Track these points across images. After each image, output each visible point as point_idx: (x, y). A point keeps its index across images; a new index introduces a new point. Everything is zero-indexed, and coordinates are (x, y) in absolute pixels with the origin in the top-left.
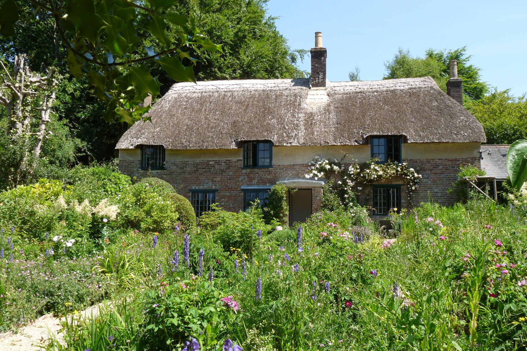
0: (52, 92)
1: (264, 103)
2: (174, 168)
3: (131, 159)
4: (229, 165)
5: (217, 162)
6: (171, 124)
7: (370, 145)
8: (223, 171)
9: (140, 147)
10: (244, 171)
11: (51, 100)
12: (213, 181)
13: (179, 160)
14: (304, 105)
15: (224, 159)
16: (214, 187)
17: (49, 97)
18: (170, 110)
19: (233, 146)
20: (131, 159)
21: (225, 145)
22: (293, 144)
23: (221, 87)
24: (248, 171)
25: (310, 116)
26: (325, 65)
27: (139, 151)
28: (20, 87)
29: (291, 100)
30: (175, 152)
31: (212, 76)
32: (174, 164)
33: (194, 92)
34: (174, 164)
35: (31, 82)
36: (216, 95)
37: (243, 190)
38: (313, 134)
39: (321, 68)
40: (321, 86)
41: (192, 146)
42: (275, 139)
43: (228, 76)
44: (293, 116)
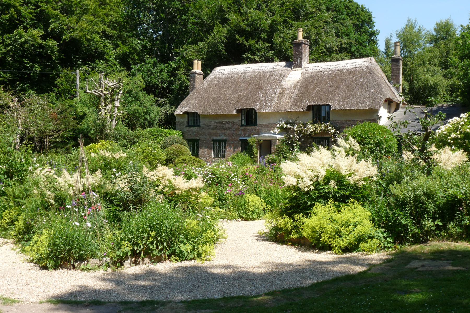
0: (120, 91)
1: (259, 82)
2: (204, 126)
3: (182, 120)
4: (233, 123)
5: (227, 122)
6: (205, 98)
7: (311, 111)
8: (230, 128)
9: (185, 113)
10: (241, 128)
11: (120, 95)
12: (224, 134)
13: (207, 121)
14: (283, 83)
15: (231, 120)
16: (225, 138)
17: (119, 93)
18: (207, 88)
19: (234, 113)
20: (182, 120)
21: (230, 111)
22: (267, 111)
23: (240, 70)
24: (244, 127)
25: (284, 90)
26: (302, 53)
27: (186, 116)
28: (102, 91)
29: (276, 79)
30: (205, 116)
31: (239, 60)
32: (204, 123)
33: (224, 74)
34: (204, 123)
35: (109, 86)
36: (236, 75)
37: (240, 140)
38: (280, 104)
39: (299, 55)
40: (299, 67)
41: (212, 113)
42: (257, 108)
43: (257, 58)
44: (274, 91)
